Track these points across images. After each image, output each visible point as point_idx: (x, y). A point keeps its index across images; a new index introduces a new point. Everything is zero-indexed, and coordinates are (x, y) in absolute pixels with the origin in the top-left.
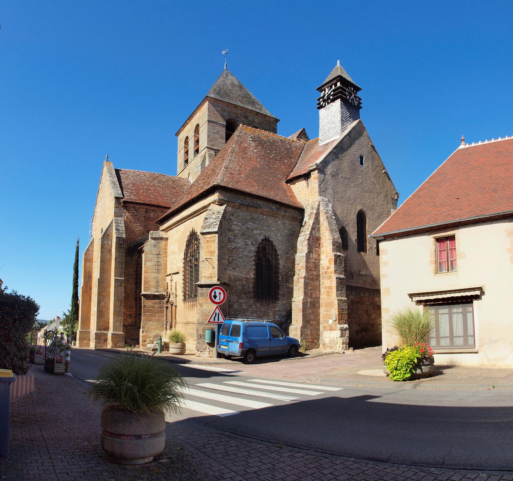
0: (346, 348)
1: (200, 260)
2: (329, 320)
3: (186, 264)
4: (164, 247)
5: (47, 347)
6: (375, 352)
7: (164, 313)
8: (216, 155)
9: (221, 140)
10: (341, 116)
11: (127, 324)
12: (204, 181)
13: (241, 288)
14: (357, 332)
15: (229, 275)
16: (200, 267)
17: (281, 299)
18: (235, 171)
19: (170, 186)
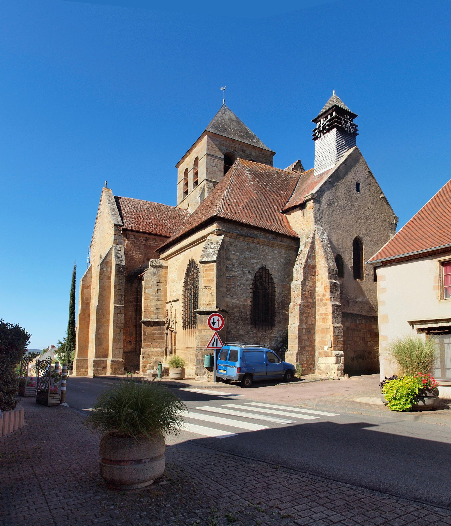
0: (341, 374)
1: (200, 288)
2: (325, 347)
3: (186, 292)
4: (164, 275)
5: (40, 378)
6: (372, 380)
7: (164, 339)
8: (214, 187)
9: (219, 173)
10: (336, 145)
11: (126, 350)
12: (204, 212)
13: (238, 315)
14: (353, 359)
15: (227, 302)
16: (199, 294)
17: (277, 325)
18: (233, 203)
19: (170, 216)
